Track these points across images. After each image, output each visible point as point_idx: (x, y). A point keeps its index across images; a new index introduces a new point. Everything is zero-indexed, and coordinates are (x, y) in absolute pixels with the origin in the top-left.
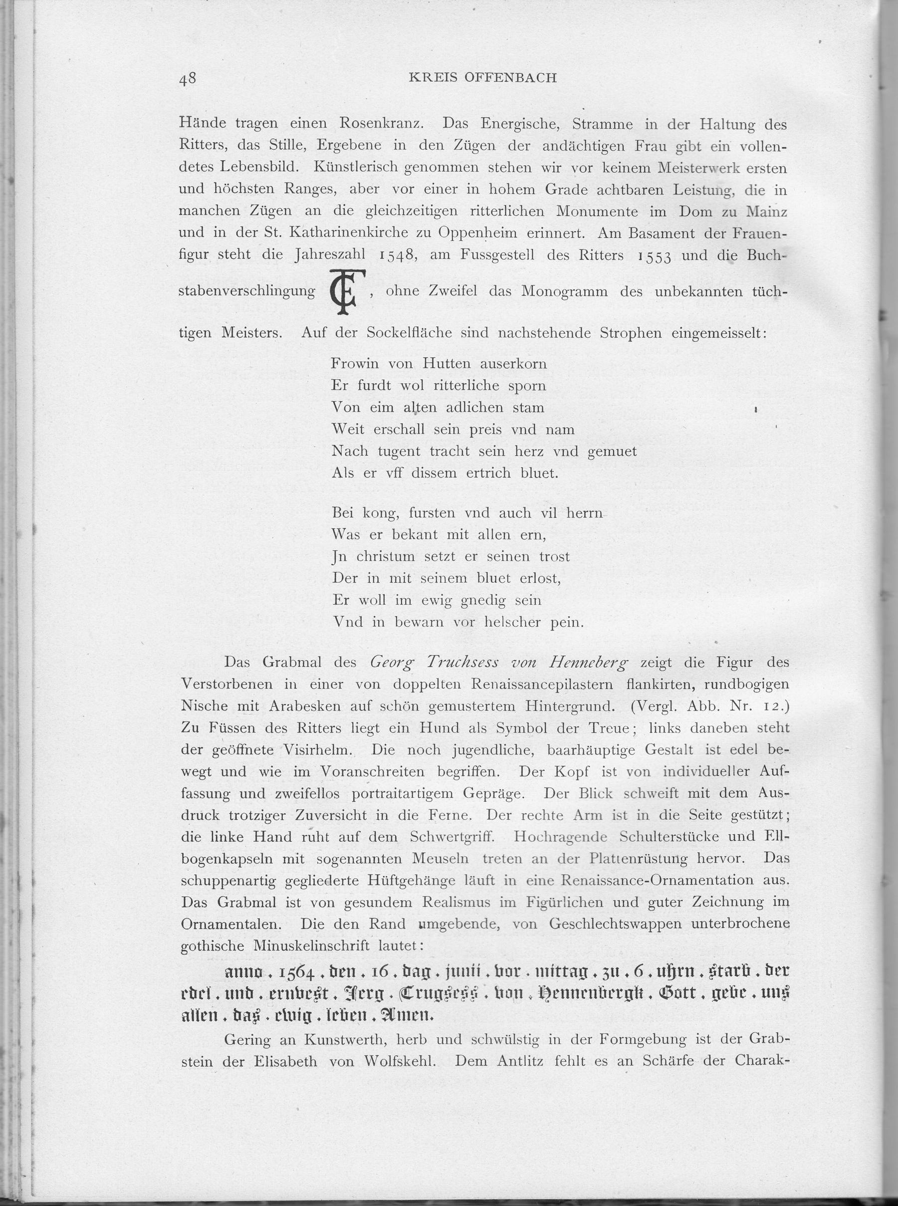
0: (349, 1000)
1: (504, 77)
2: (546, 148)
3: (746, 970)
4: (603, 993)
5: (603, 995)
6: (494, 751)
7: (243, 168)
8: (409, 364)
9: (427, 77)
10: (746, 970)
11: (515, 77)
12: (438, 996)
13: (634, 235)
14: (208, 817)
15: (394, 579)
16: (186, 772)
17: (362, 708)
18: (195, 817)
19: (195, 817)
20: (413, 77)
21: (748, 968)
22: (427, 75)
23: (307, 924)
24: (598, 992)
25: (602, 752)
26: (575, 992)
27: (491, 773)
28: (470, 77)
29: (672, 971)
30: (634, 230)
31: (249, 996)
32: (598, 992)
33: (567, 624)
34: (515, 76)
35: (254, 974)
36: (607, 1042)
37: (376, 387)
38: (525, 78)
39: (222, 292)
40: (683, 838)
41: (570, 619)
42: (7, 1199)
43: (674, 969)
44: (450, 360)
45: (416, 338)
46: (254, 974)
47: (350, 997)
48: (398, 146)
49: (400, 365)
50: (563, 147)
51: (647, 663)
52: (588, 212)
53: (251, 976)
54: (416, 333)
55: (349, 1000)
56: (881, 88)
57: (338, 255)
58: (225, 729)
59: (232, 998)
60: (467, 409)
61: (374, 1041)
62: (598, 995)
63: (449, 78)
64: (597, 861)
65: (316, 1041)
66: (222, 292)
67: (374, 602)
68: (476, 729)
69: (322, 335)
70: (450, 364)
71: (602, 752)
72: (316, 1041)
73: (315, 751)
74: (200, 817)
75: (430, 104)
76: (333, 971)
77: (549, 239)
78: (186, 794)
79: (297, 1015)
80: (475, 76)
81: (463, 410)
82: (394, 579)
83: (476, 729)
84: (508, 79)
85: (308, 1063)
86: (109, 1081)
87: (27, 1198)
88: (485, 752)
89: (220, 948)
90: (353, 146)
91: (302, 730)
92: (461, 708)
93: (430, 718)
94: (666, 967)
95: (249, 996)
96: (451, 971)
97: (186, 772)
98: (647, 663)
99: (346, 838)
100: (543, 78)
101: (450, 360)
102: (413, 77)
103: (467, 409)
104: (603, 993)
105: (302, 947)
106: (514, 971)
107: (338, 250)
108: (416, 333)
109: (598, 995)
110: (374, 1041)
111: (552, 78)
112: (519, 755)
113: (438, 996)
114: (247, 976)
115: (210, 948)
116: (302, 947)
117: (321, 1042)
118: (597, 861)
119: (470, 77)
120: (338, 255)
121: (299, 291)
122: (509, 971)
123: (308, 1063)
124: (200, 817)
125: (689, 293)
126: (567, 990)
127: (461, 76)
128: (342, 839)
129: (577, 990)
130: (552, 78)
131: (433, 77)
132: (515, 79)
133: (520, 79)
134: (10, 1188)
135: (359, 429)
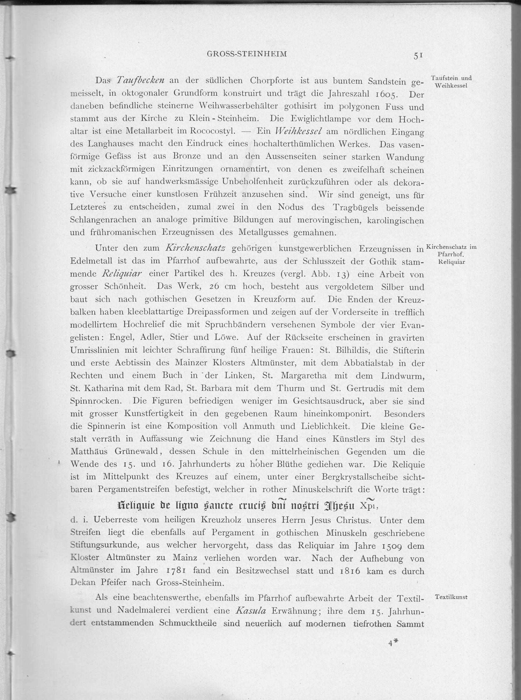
0: (327, 510)
4: (139, 507)
5: (139, 505)
8: (289, 169)
9: (215, 54)
12: (184, 507)
23: (365, 426)
24: (142, 507)
25: (345, 415)
29: (335, 506)
31: (196, 507)
32: (142, 507)
33: (168, 132)
35: (193, 507)
36: (156, 402)
40: (84, 157)
41: (155, 272)
43: (337, 504)
46: (193, 507)
47: (328, 508)
53: (219, 508)
55: (327, 510)
57: (354, 95)
59: (281, 508)
61: (293, 144)
62: (142, 505)
71: (345, 415)
79: (147, 505)
84: (260, 55)
85: (296, 106)
94: (142, 509)
95: (196, 507)
104: (139, 507)
105: (109, 401)
107: (353, 91)
109: (142, 505)
110: (293, 144)
112: (379, 480)
113: (184, 507)
114: (278, 508)
116: (109, 401)
123: (296, 106)
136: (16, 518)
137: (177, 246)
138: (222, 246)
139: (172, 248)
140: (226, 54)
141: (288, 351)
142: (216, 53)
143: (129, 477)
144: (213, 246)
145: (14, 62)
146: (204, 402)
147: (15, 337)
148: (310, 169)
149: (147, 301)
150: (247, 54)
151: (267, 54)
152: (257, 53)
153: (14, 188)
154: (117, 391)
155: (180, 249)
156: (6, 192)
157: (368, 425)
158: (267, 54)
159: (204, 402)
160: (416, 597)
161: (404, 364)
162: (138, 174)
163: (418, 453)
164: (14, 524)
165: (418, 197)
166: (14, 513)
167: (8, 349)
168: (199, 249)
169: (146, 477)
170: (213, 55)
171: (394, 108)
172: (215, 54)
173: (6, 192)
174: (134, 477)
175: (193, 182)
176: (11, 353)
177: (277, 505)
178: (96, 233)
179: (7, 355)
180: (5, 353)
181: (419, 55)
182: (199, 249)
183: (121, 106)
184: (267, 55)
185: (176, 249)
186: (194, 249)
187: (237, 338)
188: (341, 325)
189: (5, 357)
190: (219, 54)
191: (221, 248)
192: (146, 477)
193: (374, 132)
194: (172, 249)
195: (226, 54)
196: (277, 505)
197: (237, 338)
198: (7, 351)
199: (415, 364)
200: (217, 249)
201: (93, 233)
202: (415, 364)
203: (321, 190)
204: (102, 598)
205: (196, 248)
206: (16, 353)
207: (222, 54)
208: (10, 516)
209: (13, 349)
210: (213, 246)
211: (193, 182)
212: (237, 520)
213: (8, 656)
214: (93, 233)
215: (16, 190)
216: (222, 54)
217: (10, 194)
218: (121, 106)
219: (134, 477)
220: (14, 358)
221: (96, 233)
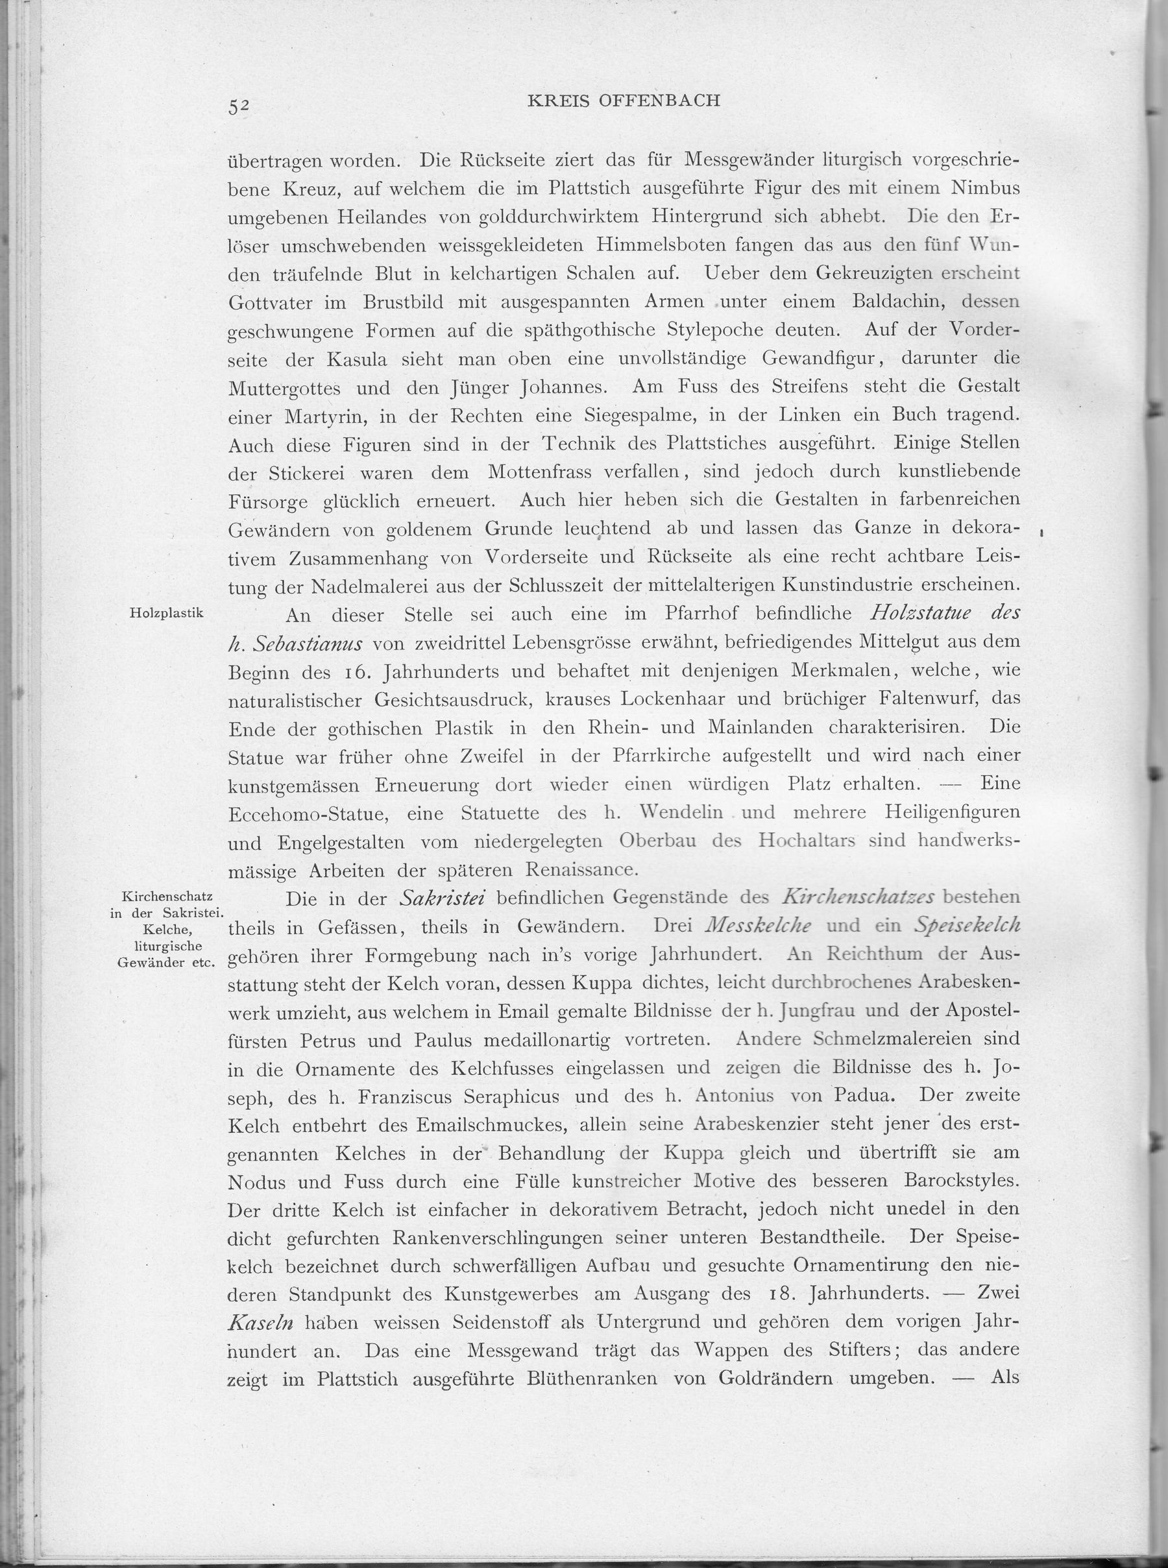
1: (650, 100)
11: (664, 100)
13: (860, 303)
14: (530, 1127)
16: (234, 1015)
17: (438, 675)
18: (496, 701)
19: (496, 701)
20: (533, 101)
22: (551, 98)
23: (236, 1211)
28: (605, 100)
30: (860, 297)
34: (665, 98)
38: (679, 101)
42: (6, 1564)
56: (1150, 113)
57: (573, 587)
58: (249, 504)
60: (816, 616)
63: (579, 102)
64: (445, 731)
65: (587, 985)
67: (657, 359)
73: (420, 674)
74: (503, 702)
75: (557, 132)
77: (737, 309)
78: (237, 758)
80: (613, 98)
81: (811, 616)
85: (600, 331)
86: (130, 1420)
87: (29, 1560)
93: (385, 688)
97: (234, 1015)
98: (580, 586)
100: (702, 100)
102: (533, 101)
103: (816, 616)
111: (713, 100)
118: (445, 731)
119: (605, 100)
121: (368, 389)
123: (600, 331)
124: (503, 702)
127: (594, 100)
130: (713, 100)
131: (558, 101)
132: (665, 102)
133: (672, 103)
134: (9, 1550)
137: (807, 893)
138: (909, 893)
139: (798, 899)
143: (346, 1296)
144: (889, 892)
146: (758, 644)
155: (814, 899)
159: (758, 644)
161: (969, 1209)
162: (737, 597)
165: (659, 162)
168: (859, 899)
169: (383, 1296)
171: (697, 389)
174: (357, 1297)
175: (306, 787)
178: (351, 759)
181: (240, 105)
182: (859, 899)
185: (806, 899)
186: (846, 899)
187: (634, 872)
191: (906, 898)
192: (383, 1296)
194: (798, 899)
197: (634, 872)
199: (996, 1209)
200: (899, 898)
201: (345, 758)
202: (996, 1209)
203: (645, 802)
204: (1005, 1380)
205: (852, 898)
210: (889, 892)
211: (306, 787)
214: (345, 758)
219: (357, 1297)
221: (351, 759)
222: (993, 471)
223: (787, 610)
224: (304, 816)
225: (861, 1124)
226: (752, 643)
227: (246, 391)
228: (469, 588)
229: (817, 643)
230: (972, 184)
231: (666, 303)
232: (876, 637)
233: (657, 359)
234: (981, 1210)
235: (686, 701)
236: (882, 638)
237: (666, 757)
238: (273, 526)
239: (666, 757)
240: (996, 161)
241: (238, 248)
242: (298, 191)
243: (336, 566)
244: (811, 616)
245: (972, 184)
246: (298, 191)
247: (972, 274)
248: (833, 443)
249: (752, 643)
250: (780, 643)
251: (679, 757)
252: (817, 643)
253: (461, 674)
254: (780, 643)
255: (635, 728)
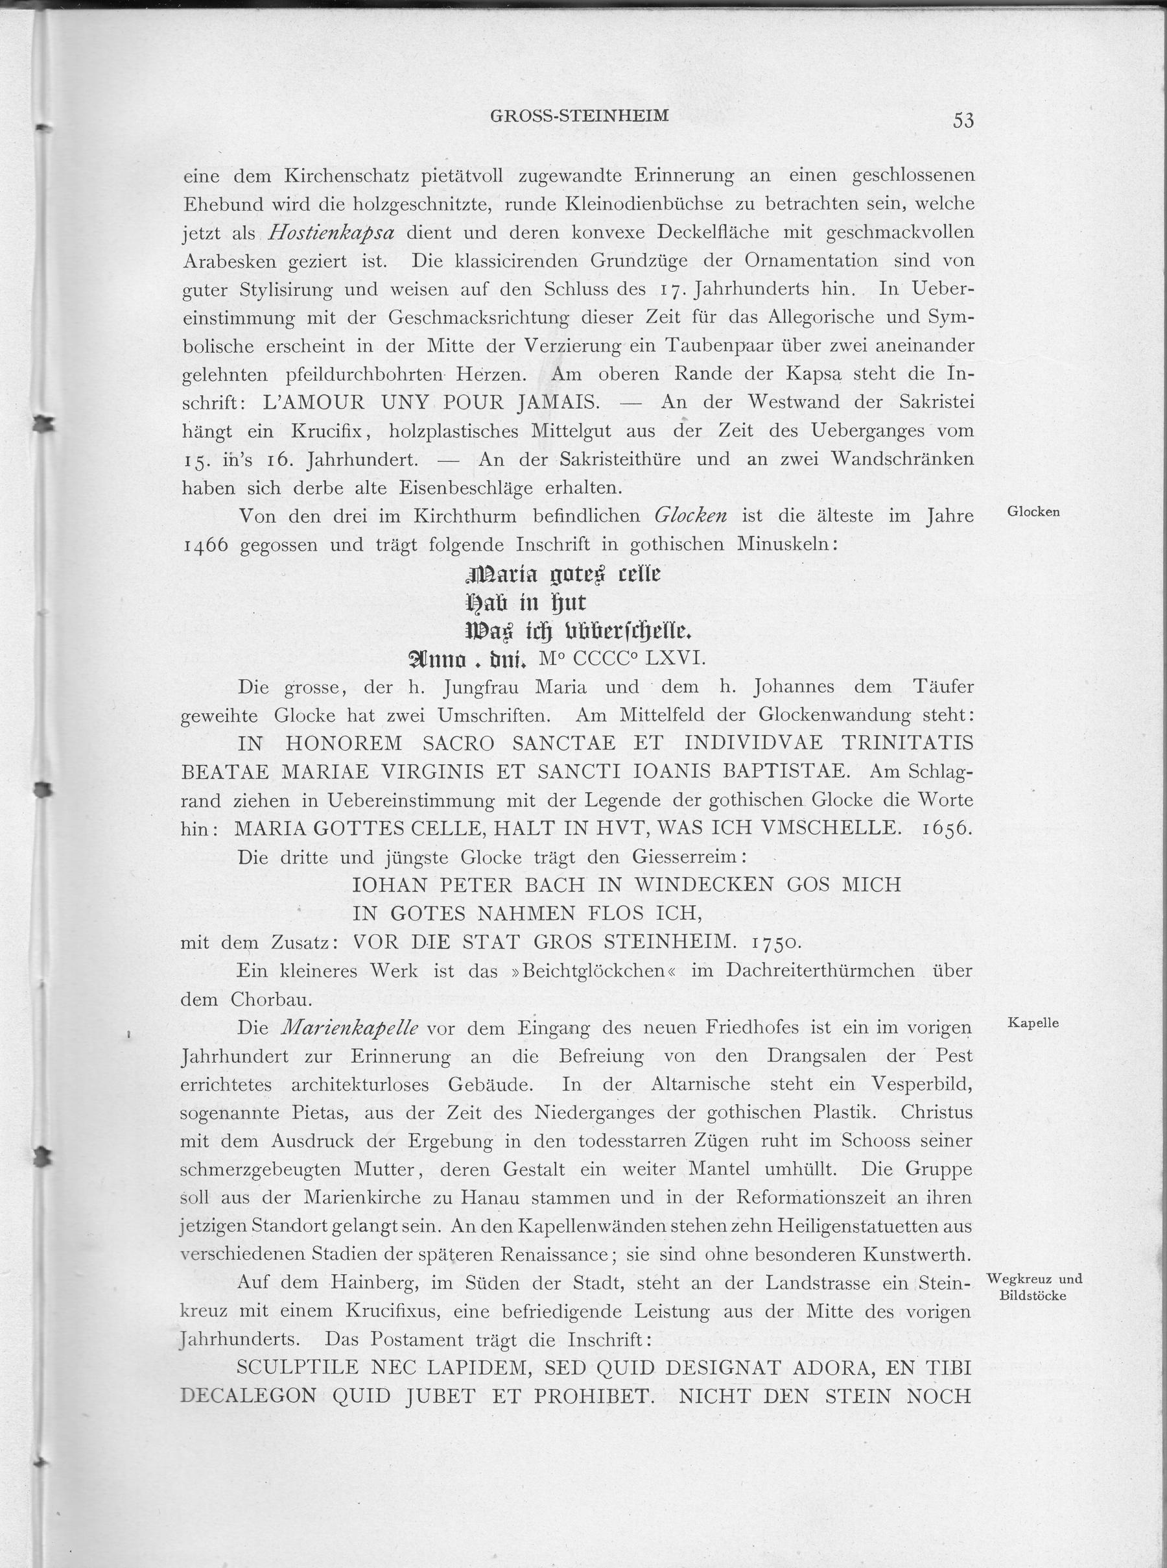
2: (369, 1116)
3: (502, 603)
6: (582, 518)
7: (843, 432)
9: (510, 116)
10: (502, 603)
15: (186, 1142)
17: (236, 1059)
21: (505, 600)
23: (420, 261)
26: (448, 659)
27: (611, 489)
37: (297, 206)
39: (605, 234)
44: (390, 1165)
45: (723, 239)
48: (607, 545)
49: (679, 1057)
50: (642, 262)
51: (863, 1199)
52: (462, 802)
54: (723, 232)
57: (856, 1200)
66: (605, 234)
67: (487, 177)
68: (242, 235)
69: (482, 292)
70: (390, 1170)
72: (878, 1257)
73: (218, 1058)
76: (495, 659)
81: (588, 519)
82: (186, 1142)
83: (242, 235)
84: (609, 118)
85: (734, 1113)
88: (633, 803)
89: (682, 546)
90: (843, 432)
91: (391, 945)
92: (237, 1200)
96: (526, 602)
98: (863, 1199)
99: (231, 1200)
101: (390, 1165)
106: (575, 573)
108: (723, 232)
115: (746, 1115)
117: (885, 1257)
120: (856, 1200)
122: (568, 573)
125: (800, 716)
126: (438, 656)
128: (466, 292)
129: (451, 656)
135: (747, 431)
136: (51, 1157)
140: (533, 116)
141: (718, 1028)
142: (511, 113)
145: (49, 137)
146: (535, 1314)
147: (52, 754)
148: (279, 1254)
149: (290, 690)
150: (581, 116)
151: (624, 115)
152: (603, 115)
153: (50, 419)
154: (918, 353)
156: (34, 429)
157: (428, 257)
158: (624, 115)
159: (535, 1314)
160: (856, 1108)
163: (330, 207)
164: (48, 1171)
166: (48, 1148)
167: (38, 781)
170: (504, 118)
172: (510, 116)
173: (34, 429)
176: (43, 789)
177: (502, 660)
179: (35, 792)
180: (32, 787)
183: (559, 517)
184: (625, 118)
187: (529, 1087)
188: (380, 376)
189: (34, 797)
190: (517, 116)
193: (859, 318)
195: (533, 116)
196: (502, 660)
197: (529, 1087)
198: (37, 784)
206: (53, 789)
207: (526, 116)
208: (40, 1153)
209: (47, 781)
212: (585, 941)
213: (36, 1469)
215: (53, 423)
216: (526, 116)
217: (41, 431)
218: (559, 517)
220: (49, 799)
222: (279, 1254)
223: (564, 512)
224: (219, 1171)
225: (800, 1085)
226: (528, 1312)
227: (371, 1171)
228: (612, 290)
229: (595, 1313)
230: (435, 513)
231: (856, 972)
232: (637, 711)
233: (487, 177)
234: (527, 1143)
235: (792, 1172)
236: (450, 342)
237: (376, 1199)
238: (198, 427)
239: (376, 1199)
240: (339, 1199)
241: (599, 972)
242: (361, 1313)
243: (424, 1347)
244: (588, 519)
245: (435, 513)
246: (361, 1313)
247: (765, 1114)
248: (698, 317)
249: (528, 1312)
250: (557, 1313)
251: (389, 1199)
252: (595, 1313)
253: (606, 1313)
254: (557, 1313)
255: (957, 1284)
